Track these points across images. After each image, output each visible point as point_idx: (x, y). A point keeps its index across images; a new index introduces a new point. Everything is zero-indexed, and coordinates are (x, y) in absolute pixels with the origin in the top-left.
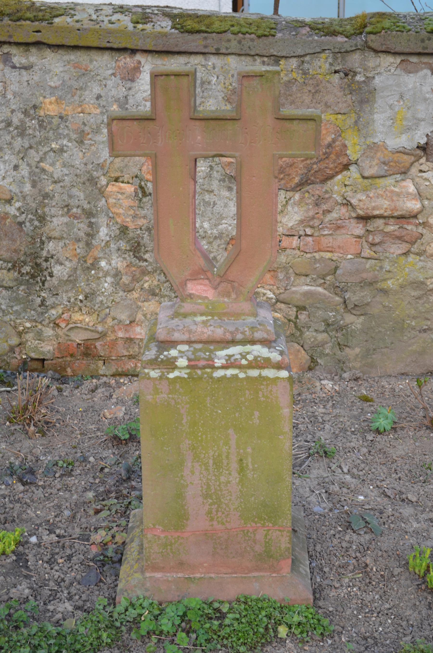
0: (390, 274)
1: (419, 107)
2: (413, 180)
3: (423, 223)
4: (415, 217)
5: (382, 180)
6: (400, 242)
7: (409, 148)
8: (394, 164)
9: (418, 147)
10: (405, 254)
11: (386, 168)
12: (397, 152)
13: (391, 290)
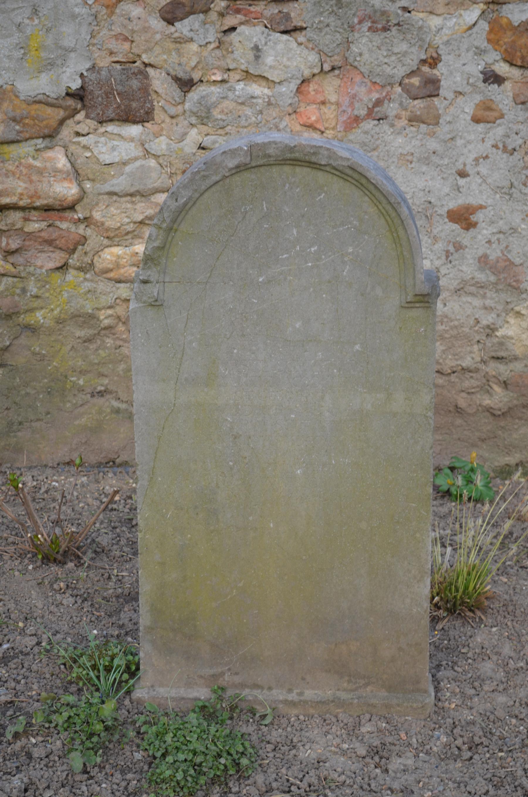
0: (39, 301)
1: (64, 29)
2: (66, 147)
3: (85, 218)
4: (72, 208)
5: (13, 147)
6: (51, 249)
7: (53, 95)
8: (32, 122)
9: (68, 94)
10: (61, 267)
11: (17, 127)
12: (36, 102)
13: (42, 326)
